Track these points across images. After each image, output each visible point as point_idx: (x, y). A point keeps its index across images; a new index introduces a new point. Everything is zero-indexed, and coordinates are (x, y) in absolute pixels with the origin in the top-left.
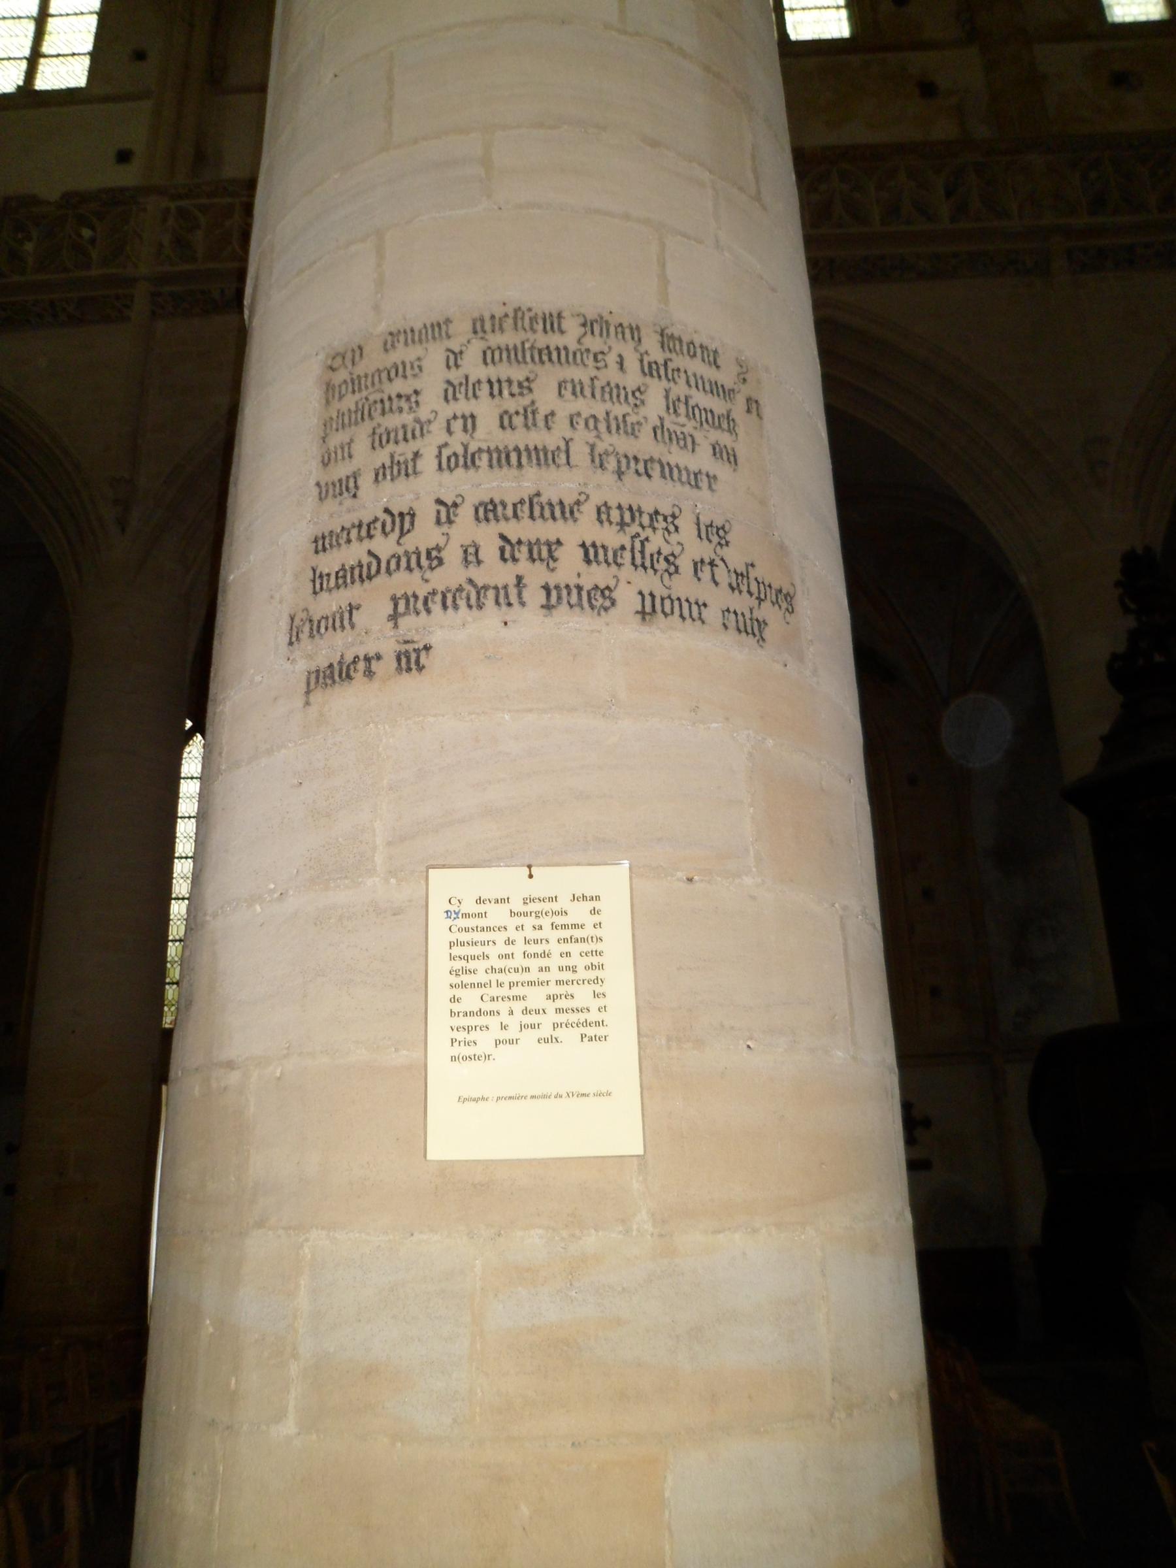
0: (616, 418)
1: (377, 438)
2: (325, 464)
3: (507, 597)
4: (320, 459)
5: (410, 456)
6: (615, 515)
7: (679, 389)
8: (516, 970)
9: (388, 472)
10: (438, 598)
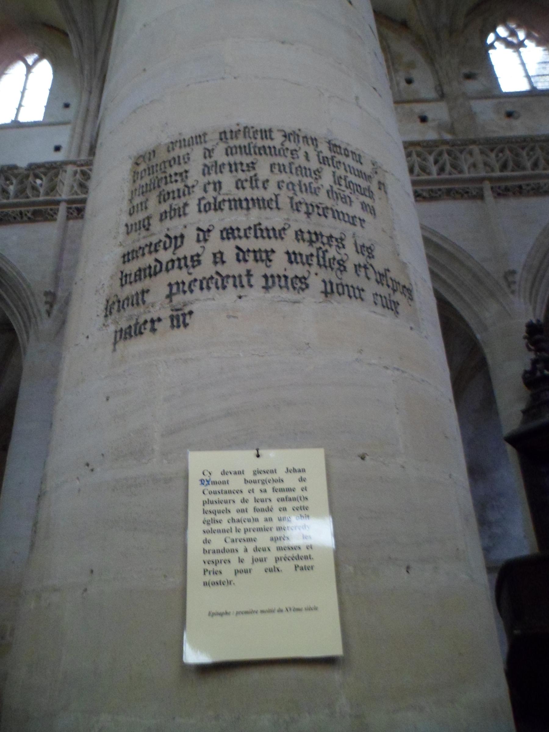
0: (305, 185)
1: (162, 197)
2: (131, 214)
3: (240, 282)
4: (128, 211)
5: (181, 205)
6: (306, 236)
7: (341, 172)
8: (249, 521)
9: (168, 215)
10: (198, 284)
